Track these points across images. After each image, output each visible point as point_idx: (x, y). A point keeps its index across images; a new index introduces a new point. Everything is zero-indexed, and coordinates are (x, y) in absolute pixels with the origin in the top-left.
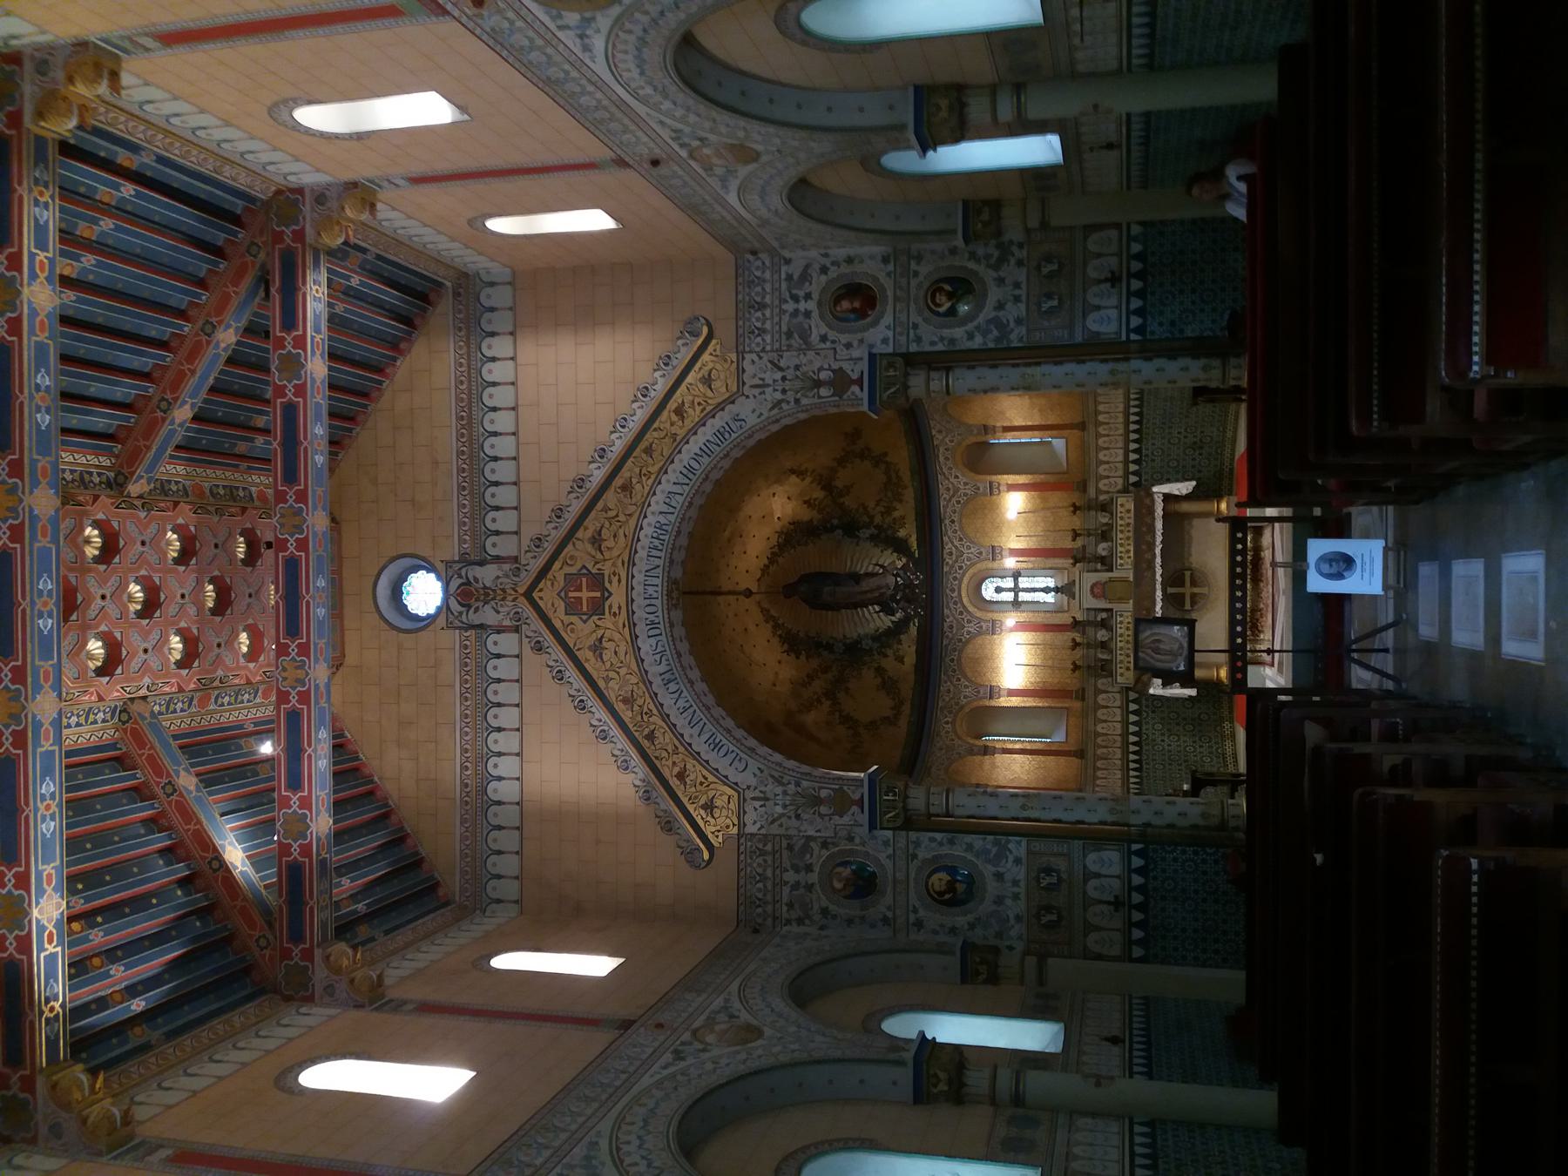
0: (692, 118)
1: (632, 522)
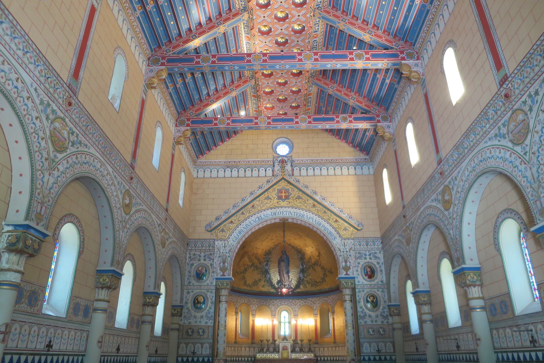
0: (417, 228)
1: (304, 208)
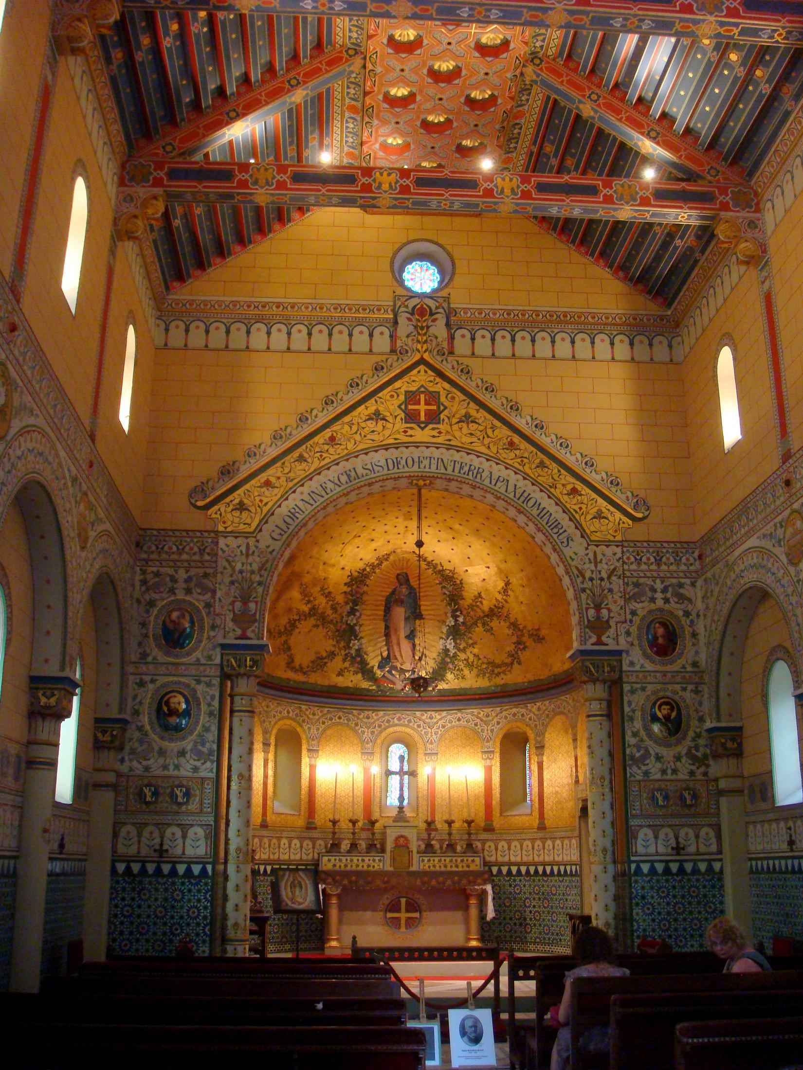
1: (484, 450)
